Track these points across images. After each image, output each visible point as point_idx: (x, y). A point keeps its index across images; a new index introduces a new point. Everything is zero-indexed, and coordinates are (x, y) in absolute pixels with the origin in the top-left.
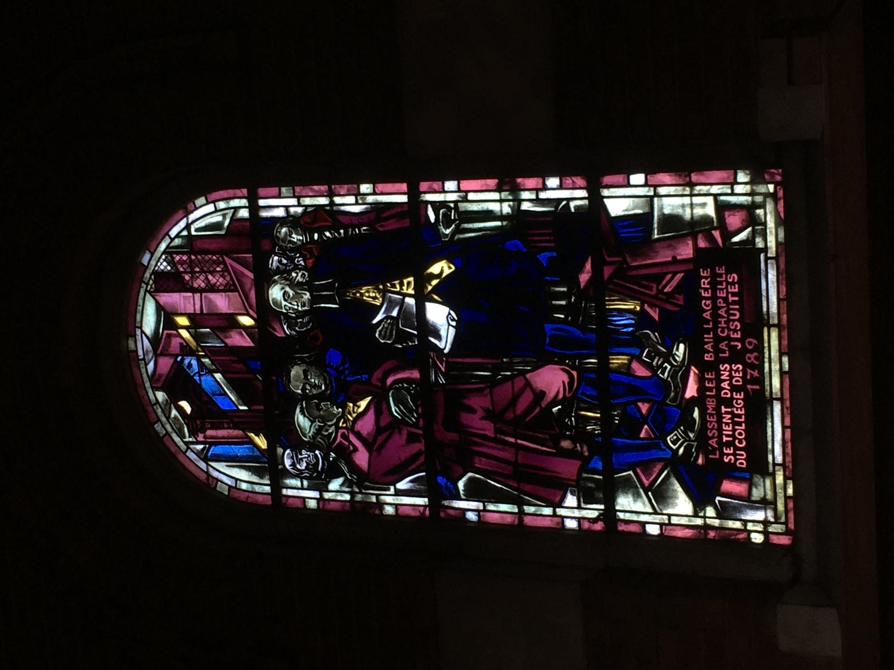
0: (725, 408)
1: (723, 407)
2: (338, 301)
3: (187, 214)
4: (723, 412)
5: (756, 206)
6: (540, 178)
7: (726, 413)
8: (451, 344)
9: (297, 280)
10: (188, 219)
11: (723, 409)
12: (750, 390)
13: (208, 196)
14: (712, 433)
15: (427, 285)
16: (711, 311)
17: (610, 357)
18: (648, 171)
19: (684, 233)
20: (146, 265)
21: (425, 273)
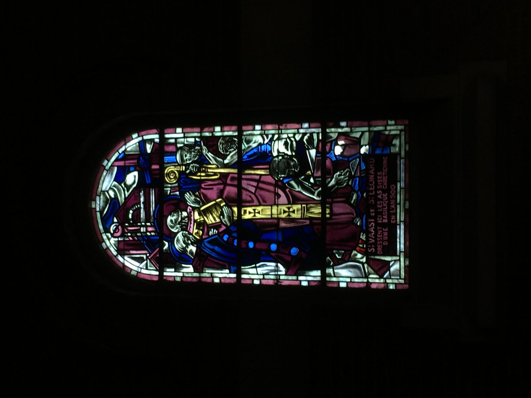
0: (379, 227)
1: (378, 227)
2: (105, 213)
3: (125, 144)
4: (378, 229)
5: (107, 226)
6: (398, 289)
7: (380, 230)
8: (144, 278)
9: (262, 152)
10: (125, 147)
11: (378, 228)
12: (354, 172)
13: (139, 133)
14: (371, 250)
15: (134, 207)
16: (327, 141)
17: (320, 216)
18: (213, 283)
19: (252, 157)
20: (337, 134)
21: (142, 189)
